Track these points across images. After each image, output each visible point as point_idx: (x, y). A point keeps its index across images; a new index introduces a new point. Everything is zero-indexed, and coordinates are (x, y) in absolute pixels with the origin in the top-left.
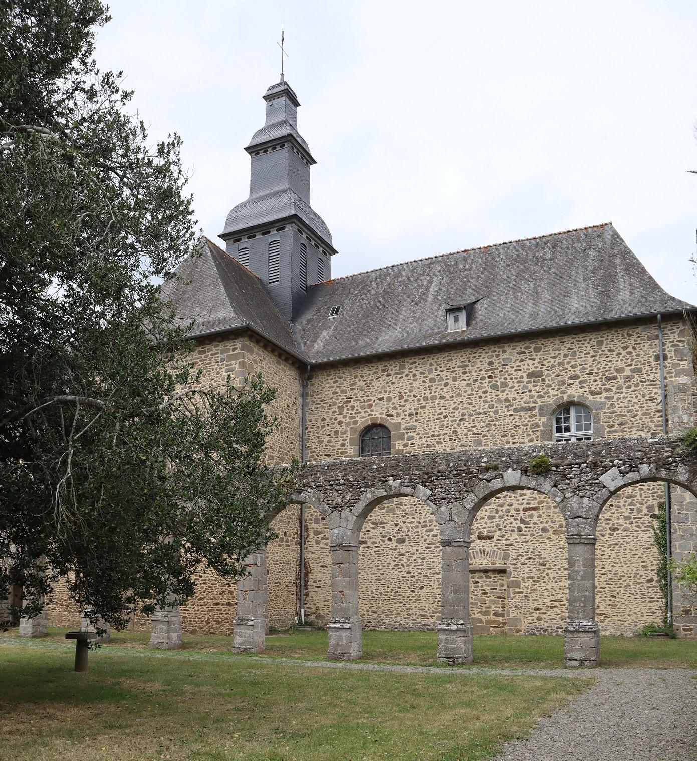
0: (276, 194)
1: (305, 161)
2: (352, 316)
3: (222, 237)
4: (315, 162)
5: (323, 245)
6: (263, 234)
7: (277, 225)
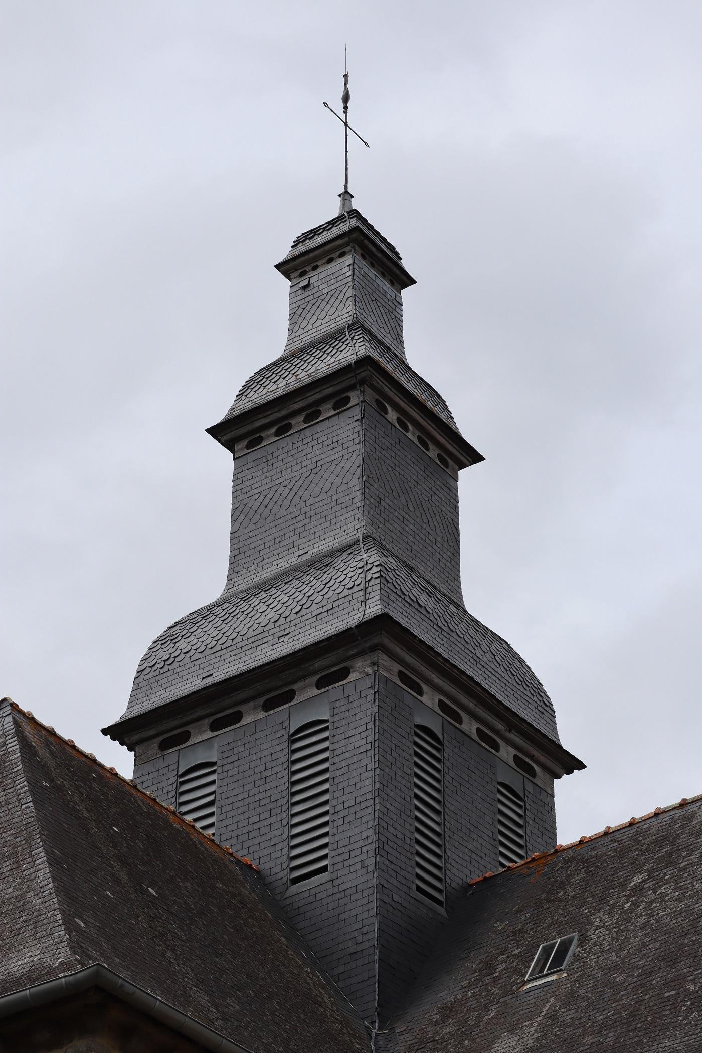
0: (321, 563)
1: (433, 453)
2: (616, 968)
3: (115, 732)
4: (477, 458)
5: (513, 736)
6: (269, 706)
7: (318, 664)
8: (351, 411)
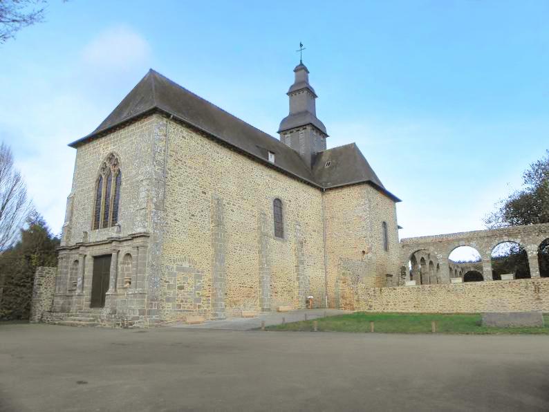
8: (302, 91)
